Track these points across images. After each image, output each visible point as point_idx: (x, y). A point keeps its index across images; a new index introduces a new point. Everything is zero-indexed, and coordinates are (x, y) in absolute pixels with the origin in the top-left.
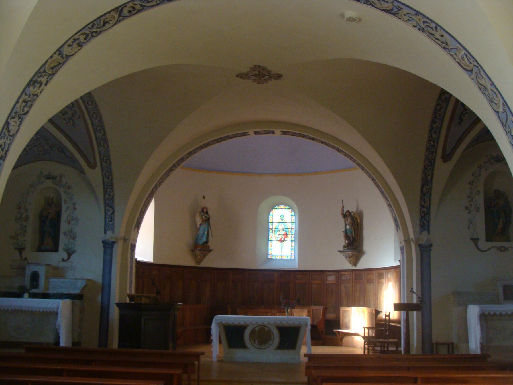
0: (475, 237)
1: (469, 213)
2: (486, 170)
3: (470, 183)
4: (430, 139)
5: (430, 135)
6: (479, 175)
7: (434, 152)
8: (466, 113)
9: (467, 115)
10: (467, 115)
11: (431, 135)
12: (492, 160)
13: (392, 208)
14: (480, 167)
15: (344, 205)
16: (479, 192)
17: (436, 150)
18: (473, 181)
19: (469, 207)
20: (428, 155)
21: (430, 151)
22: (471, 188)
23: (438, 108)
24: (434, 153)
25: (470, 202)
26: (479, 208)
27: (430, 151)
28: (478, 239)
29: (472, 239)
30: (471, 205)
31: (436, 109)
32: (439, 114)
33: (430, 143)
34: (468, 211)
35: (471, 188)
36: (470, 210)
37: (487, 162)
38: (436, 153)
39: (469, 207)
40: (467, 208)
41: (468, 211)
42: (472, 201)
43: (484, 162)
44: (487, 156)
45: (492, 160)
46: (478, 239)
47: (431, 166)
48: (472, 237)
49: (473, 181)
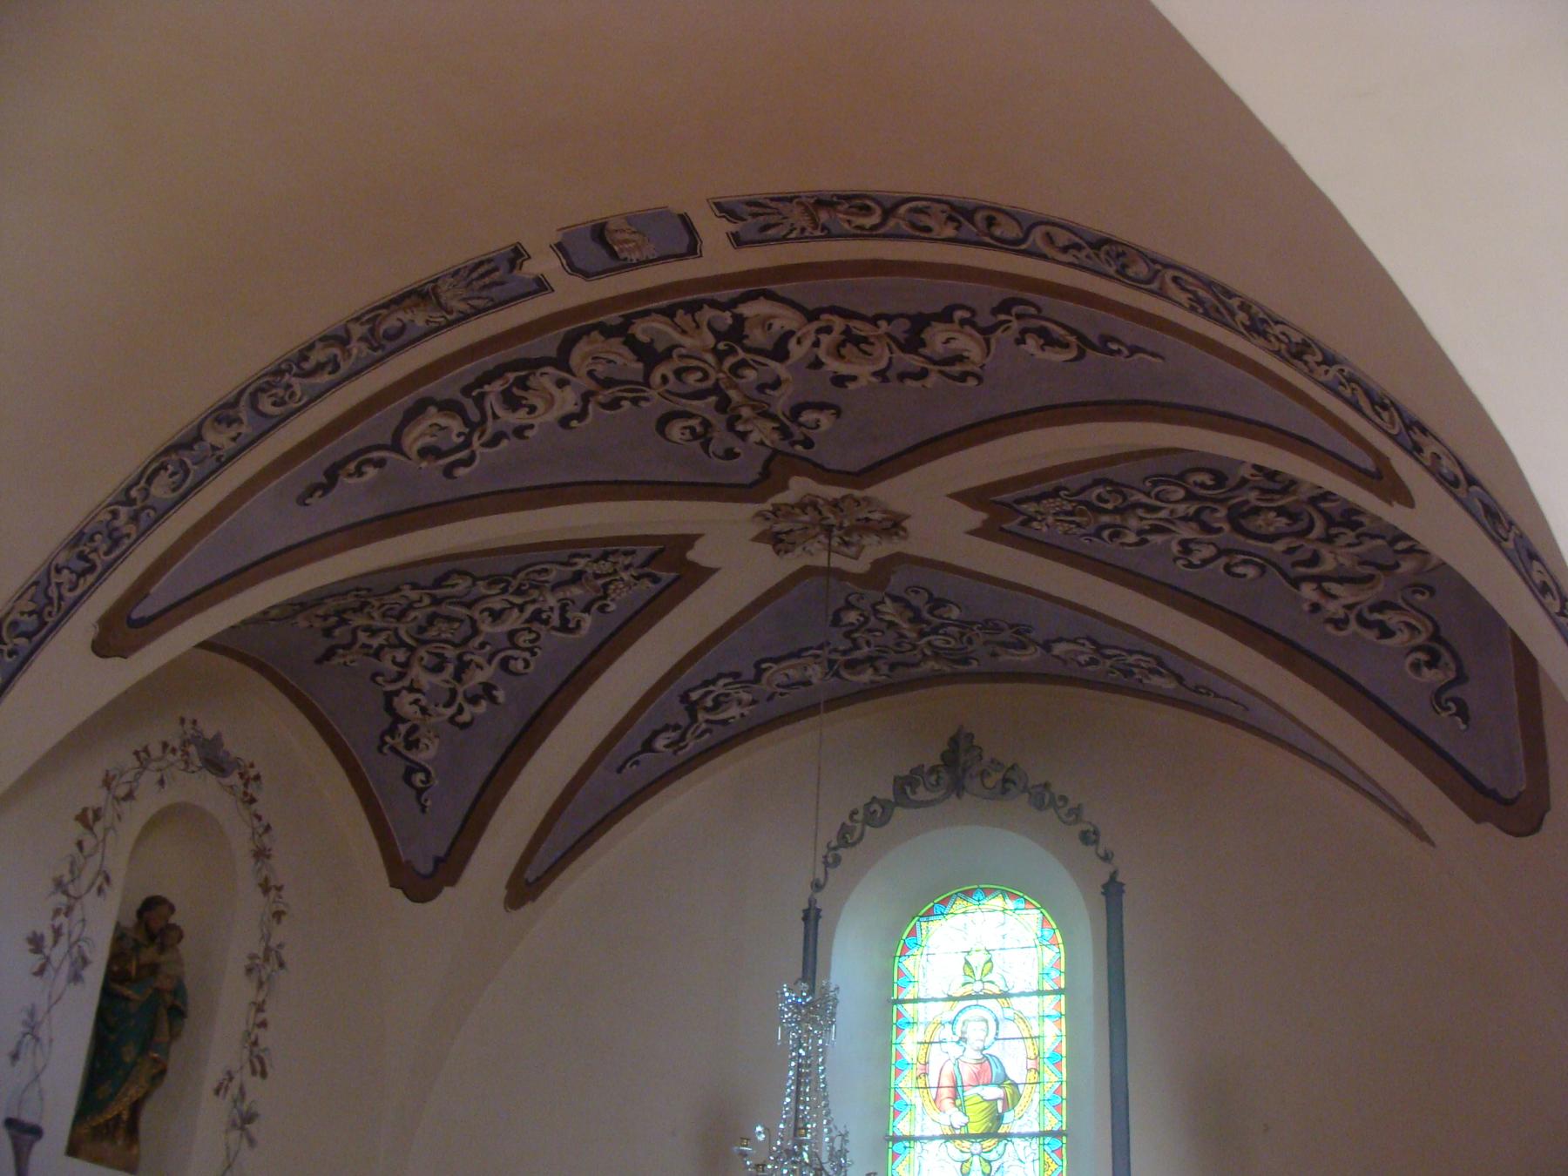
0: (28, 1117)
1: (40, 972)
2: (162, 782)
3: (82, 818)
4: (134, 493)
5: (148, 476)
6: (129, 796)
7: (93, 568)
8: (380, 463)
9: (371, 472)
10: (371, 472)
11: (156, 472)
12: (192, 749)
13: (952, 895)
14: (143, 757)
15: (699, 683)
16: (107, 879)
17: (110, 567)
18: (97, 814)
19: (49, 940)
20: (58, 571)
21: (82, 557)
22: (80, 845)
23: (318, 356)
24: (90, 578)
25: (57, 912)
26: (85, 962)
27: (82, 557)
28: (36, 1132)
29: (10, 1123)
30: (57, 932)
31: (303, 355)
32: (289, 386)
33: (115, 514)
34: (35, 960)
35: (80, 845)
36: (48, 959)
37: (174, 751)
38: (100, 579)
39: (49, 940)
40: (36, 943)
41: (35, 960)
42: (69, 911)
43: (165, 745)
44: (183, 721)
45: (192, 749)
46: (36, 1132)
47: (28, 635)
48: (14, 1115)
49: (97, 814)
